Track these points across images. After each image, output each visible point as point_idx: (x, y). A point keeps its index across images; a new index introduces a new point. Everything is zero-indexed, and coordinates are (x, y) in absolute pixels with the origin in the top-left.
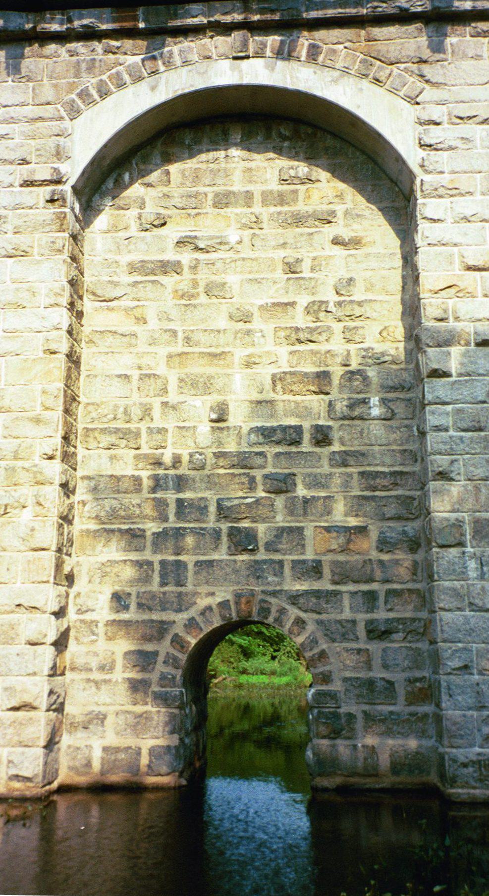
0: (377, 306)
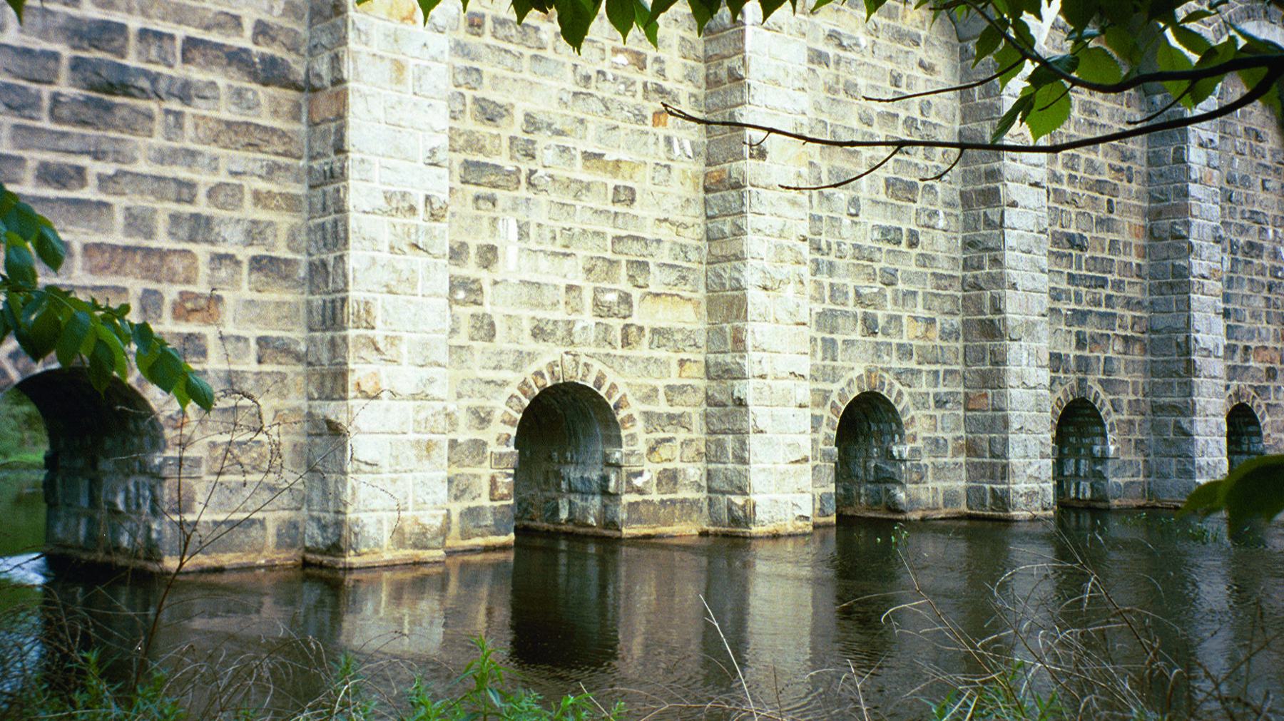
0: (942, 130)
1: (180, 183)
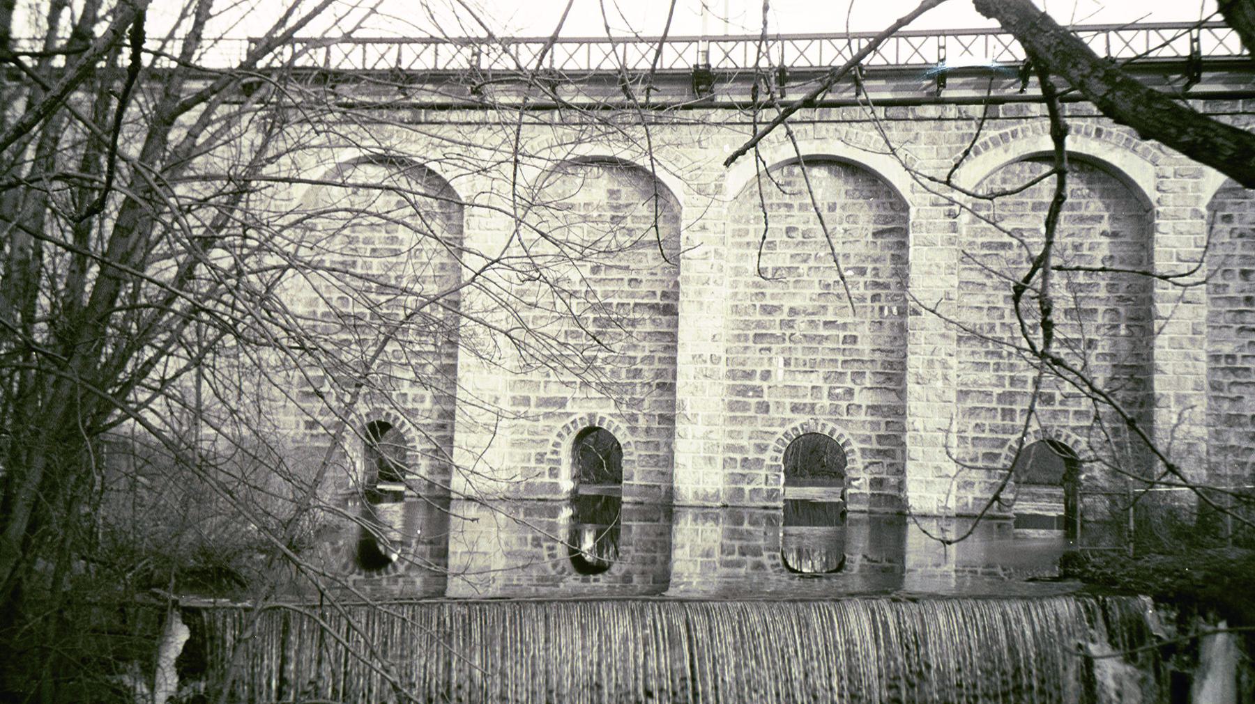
1: (630, 357)
